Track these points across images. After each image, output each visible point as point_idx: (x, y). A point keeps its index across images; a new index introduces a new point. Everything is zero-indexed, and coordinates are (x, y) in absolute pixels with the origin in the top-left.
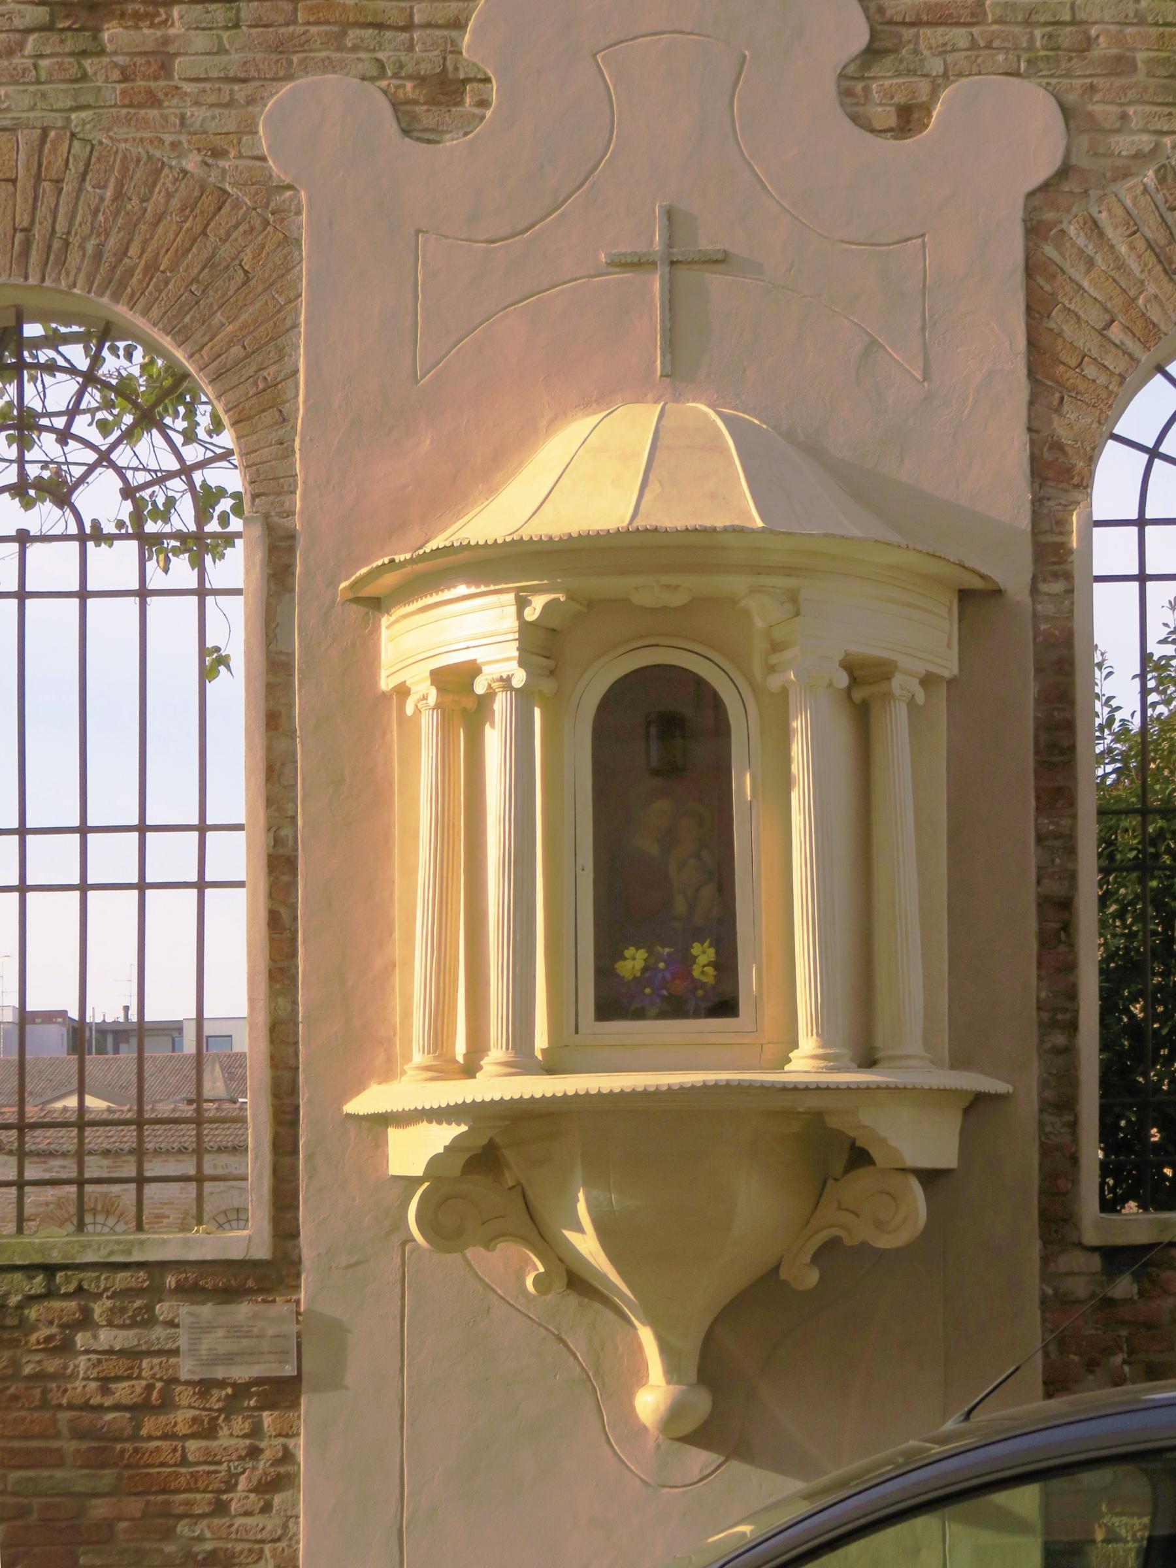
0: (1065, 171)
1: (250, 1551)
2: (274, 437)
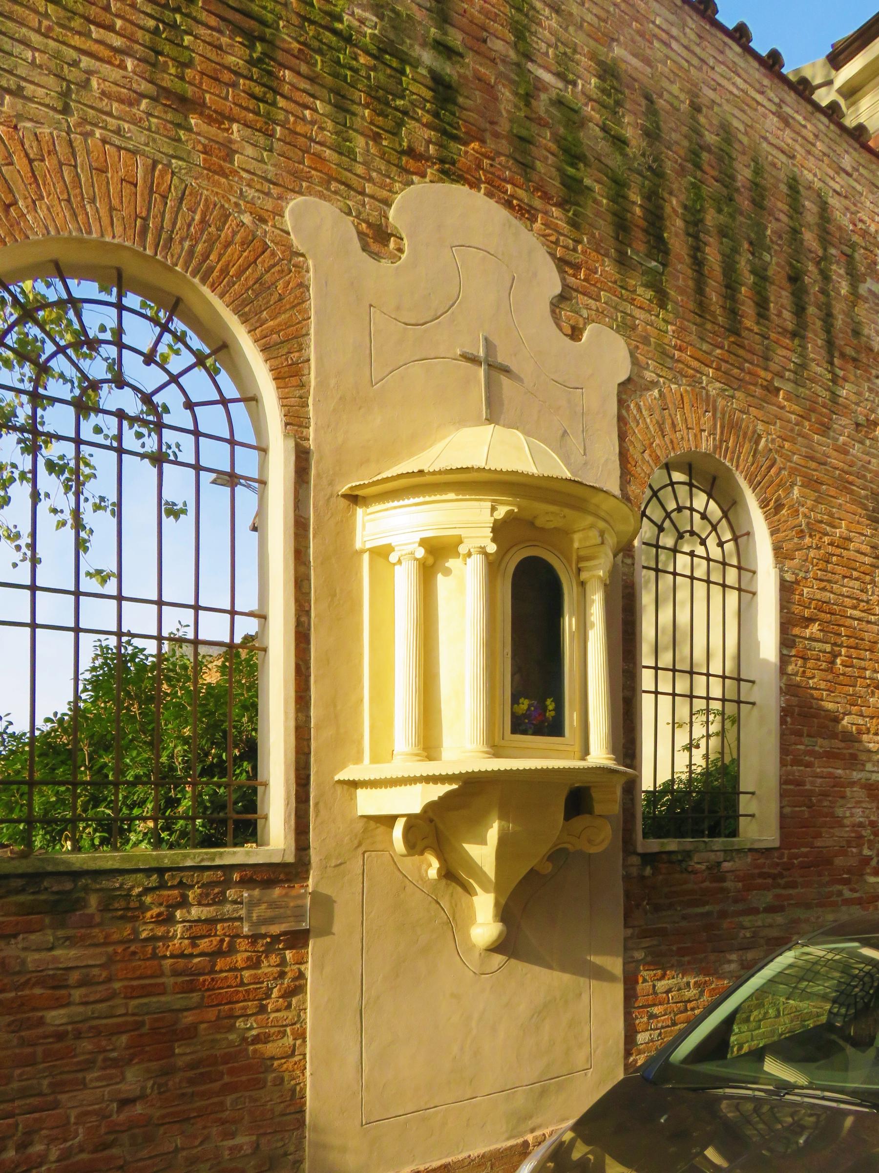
0: (629, 380)
1: (279, 1032)
2: (298, 393)
